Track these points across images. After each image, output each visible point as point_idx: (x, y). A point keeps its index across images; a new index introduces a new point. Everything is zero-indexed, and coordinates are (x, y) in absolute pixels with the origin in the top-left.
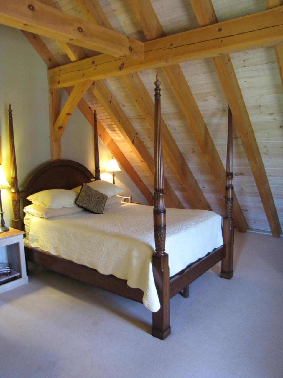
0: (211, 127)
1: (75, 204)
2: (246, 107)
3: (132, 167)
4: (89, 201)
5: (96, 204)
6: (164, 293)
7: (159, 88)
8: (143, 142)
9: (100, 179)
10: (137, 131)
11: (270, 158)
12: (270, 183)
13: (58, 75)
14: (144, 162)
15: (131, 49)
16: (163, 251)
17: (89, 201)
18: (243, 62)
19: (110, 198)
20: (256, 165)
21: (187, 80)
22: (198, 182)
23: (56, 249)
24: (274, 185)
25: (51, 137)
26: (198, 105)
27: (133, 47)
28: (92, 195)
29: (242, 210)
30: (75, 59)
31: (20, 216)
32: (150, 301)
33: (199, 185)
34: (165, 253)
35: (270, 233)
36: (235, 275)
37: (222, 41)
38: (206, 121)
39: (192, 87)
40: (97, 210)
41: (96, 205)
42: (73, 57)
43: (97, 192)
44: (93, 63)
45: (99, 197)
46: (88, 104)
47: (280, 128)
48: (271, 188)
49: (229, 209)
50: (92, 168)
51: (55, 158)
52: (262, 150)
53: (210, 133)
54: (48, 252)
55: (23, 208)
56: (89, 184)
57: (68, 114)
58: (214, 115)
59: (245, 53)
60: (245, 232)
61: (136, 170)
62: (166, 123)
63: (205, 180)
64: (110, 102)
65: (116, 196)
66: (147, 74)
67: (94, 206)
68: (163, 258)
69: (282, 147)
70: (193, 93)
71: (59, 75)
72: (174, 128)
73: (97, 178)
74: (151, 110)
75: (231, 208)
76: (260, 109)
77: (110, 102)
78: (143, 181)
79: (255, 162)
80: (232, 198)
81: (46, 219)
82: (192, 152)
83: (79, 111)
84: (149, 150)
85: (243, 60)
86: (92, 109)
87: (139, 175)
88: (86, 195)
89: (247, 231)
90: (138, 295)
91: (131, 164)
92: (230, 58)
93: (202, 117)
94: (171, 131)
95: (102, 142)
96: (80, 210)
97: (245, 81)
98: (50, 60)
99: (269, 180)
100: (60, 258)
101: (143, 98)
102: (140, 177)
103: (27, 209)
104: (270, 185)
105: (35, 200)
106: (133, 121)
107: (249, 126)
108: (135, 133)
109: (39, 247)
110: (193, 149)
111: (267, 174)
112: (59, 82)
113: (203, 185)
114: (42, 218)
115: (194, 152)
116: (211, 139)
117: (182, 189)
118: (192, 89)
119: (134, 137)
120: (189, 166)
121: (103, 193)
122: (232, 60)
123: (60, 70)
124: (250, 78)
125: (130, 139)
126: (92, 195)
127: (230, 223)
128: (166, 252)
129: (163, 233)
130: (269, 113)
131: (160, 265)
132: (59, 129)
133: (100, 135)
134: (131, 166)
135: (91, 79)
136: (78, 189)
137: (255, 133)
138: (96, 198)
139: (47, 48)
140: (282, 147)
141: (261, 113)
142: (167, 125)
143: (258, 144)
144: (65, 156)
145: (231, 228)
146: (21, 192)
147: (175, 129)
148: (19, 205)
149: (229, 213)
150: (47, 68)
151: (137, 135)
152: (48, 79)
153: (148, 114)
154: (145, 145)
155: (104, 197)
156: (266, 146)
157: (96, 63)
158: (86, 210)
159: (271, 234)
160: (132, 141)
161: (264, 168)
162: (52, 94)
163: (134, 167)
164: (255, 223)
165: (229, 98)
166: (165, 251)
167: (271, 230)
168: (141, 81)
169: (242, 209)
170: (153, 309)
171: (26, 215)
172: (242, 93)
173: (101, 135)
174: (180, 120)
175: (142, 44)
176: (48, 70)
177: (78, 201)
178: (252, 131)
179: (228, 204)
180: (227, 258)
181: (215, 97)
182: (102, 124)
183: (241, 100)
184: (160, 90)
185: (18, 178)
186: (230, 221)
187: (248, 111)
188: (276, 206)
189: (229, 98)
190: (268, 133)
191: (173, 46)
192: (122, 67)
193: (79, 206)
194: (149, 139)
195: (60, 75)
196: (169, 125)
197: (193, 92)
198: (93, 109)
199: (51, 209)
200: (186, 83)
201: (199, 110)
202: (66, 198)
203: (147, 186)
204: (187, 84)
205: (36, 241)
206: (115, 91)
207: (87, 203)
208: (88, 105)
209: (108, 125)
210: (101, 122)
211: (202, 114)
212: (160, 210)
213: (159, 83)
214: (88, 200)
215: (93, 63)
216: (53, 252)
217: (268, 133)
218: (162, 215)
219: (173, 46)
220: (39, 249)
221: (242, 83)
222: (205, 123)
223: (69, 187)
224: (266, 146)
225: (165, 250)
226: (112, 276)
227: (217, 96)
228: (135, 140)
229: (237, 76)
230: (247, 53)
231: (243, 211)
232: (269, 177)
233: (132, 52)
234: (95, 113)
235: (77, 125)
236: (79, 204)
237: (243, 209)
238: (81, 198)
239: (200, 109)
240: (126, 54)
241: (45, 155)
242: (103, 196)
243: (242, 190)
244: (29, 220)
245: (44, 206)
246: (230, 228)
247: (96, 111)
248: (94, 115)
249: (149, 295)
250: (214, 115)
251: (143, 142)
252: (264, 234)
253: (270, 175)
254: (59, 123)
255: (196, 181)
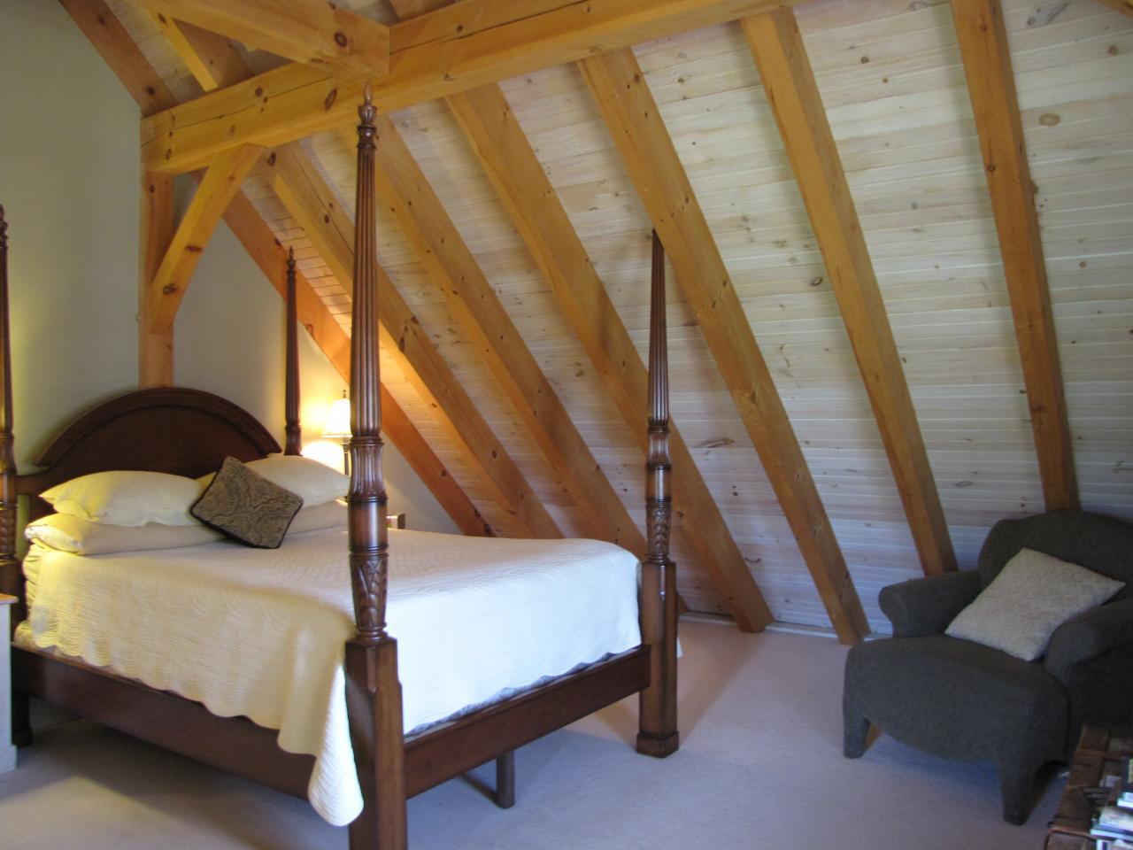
0: (619, 290)
1: (191, 517)
2: (709, 223)
3: (413, 431)
4: (236, 509)
5: (257, 518)
6: (382, 766)
7: (369, 126)
8: (436, 347)
9: (298, 454)
10: (415, 313)
11: (799, 387)
12: (811, 467)
13: (168, 134)
14: (439, 407)
15: (340, 39)
16: (376, 628)
17: (236, 509)
18: (679, 84)
19: (312, 508)
20: (753, 406)
21: (533, 145)
22: (606, 472)
23: (101, 645)
24: (825, 474)
25: (140, 318)
26: (573, 224)
27: (348, 33)
28: (248, 490)
29: (747, 559)
30: (214, 85)
31: (14, 552)
32: (328, 791)
33: (611, 482)
34: (384, 635)
35: (830, 632)
36: (684, 746)
37: (589, 10)
38: (601, 271)
39: (549, 168)
40: (261, 537)
41: (259, 521)
42: (207, 80)
43: (270, 483)
44: (259, 92)
45: (272, 499)
46: (273, 230)
47: (813, 288)
48: (818, 486)
49: (658, 534)
50: (275, 423)
51: (153, 382)
52: (773, 363)
53: (620, 312)
54: (79, 657)
55: (24, 527)
56: (257, 467)
57: (192, 249)
58: (620, 253)
59: (680, 56)
60: (762, 630)
61: (427, 438)
62: (491, 282)
63: (625, 465)
64: (327, 219)
65: (337, 503)
66: (422, 130)
67: (251, 525)
68: (374, 648)
69: (827, 350)
70: (554, 186)
71: (171, 134)
72: (517, 299)
73: (293, 449)
74: (440, 240)
75: (664, 530)
76: (748, 229)
77: (327, 219)
78: (453, 475)
79: (748, 395)
80: (668, 499)
81: (85, 555)
82: (577, 375)
83: (241, 248)
84: (454, 371)
85: (677, 77)
86: (283, 244)
87: (438, 456)
88: (229, 491)
89: (768, 628)
90: (296, 774)
91: (410, 420)
92: (642, 73)
93: (587, 260)
94: (509, 309)
95: (316, 348)
96: (207, 535)
97: (694, 143)
98: (151, 91)
99: (807, 458)
100: (111, 675)
101: (413, 203)
102: (442, 460)
103: (40, 529)
104: (814, 476)
105: (65, 498)
106: (400, 280)
107: (721, 284)
108: (409, 317)
109: (59, 645)
110: (579, 365)
111: (800, 437)
112: (168, 155)
113: (622, 484)
114: (75, 553)
115: (580, 374)
116: (623, 332)
117: (564, 499)
118: (549, 173)
119: (406, 329)
120: (575, 423)
121: (288, 489)
122: (646, 77)
123: (174, 118)
124: (704, 131)
125: (393, 337)
126: (248, 490)
127: (659, 580)
128: (390, 630)
129: (375, 567)
130: (773, 242)
131: (365, 670)
132: (165, 293)
133: (309, 327)
134: (412, 426)
135: (254, 139)
136: (208, 479)
137: (743, 305)
138: (259, 502)
139: (143, 57)
140: (827, 350)
141: (752, 241)
142: (494, 292)
143: (758, 341)
144: (186, 376)
145: (666, 590)
146: (20, 476)
147: (520, 303)
148: (14, 517)
149: (658, 545)
150: (139, 114)
151: (415, 326)
152: (142, 146)
153: (428, 251)
154: (444, 357)
155: (289, 499)
156: (781, 348)
157: (265, 94)
158: (230, 538)
159: (835, 636)
160: (399, 340)
161: (787, 418)
162: (152, 189)
163: (420, 431)
164: (787, 601)
165: (646, 190)
166: (385, 629)
167: (833, 621)
168: (407, 153)
169: (744, 556)
170: (335, 817)
171: (32, 547)
172: (691, 181)
173: (315, 326)
174: (529, 272)
175: (385, 30)
176: (142, 118)
177: (201, 507)
178: (735, 302)
179: (655, 517)
180: (654, 689)
181: (617, 195)
182: (315, 294)
183: (687, 201)
184: (373, 129)
185: (15, 431)
186: (660, 569)
187: (714, 236)
188: (842, 543)
189: (646, 190)
190: (781, 306)
191: (464, 32)
192: (331, 101)
193: (207, 525)
194: (451, 338)
195: (174, 131)
196: (500, 291)
197: (555, 182)
198: (286, 246)
199: (106, 526)
200: (530, 153)
201: (578, 241)
202: (165, 498)
203: (465, 491)
204: (535, 159)
205: (51, 625)
206: (341, 186)
207: (230, 515)
208: (272, 233)
209: (333, 295)
210: (313, 286)
211: (588, 251)
212: (365, 494)
213: (369, 111)
214: (232, 504)
215: (259, 92)
216: (93, 659)
217: (781, 306)
218: (374, 508)
219: (464, 32)
220: (57, 654)
221: (688, 151)
222: (602, 279)
223: (194, 475)
224: (781, 348)
225: (384, 624)
226: (243, 720)
227: (620, 193)
228: (409, 338)
229: (670, 129)
230: (682, 56)
231: (749, 565)
232: (805, 450)
233: (347, 48)
234: (291, 257)
235: (228, 290)
236: (201, 515)
237: (749, 558)
238: (210, 498)
239: (581, 234)
240: (325, 52)
241: (119, 369)
242: (288, 497)
243: (735, 494)
244: (38, 563)
245: (85, 516)
246: (660, 591)
247: (295, 252)
248: (288, 262)
249: (326, 771)
250: (620, 253)
251: (436, 347)
252: (799, 635)
253: (807, 442)
254: (165, 277)
255: (598, 467)
